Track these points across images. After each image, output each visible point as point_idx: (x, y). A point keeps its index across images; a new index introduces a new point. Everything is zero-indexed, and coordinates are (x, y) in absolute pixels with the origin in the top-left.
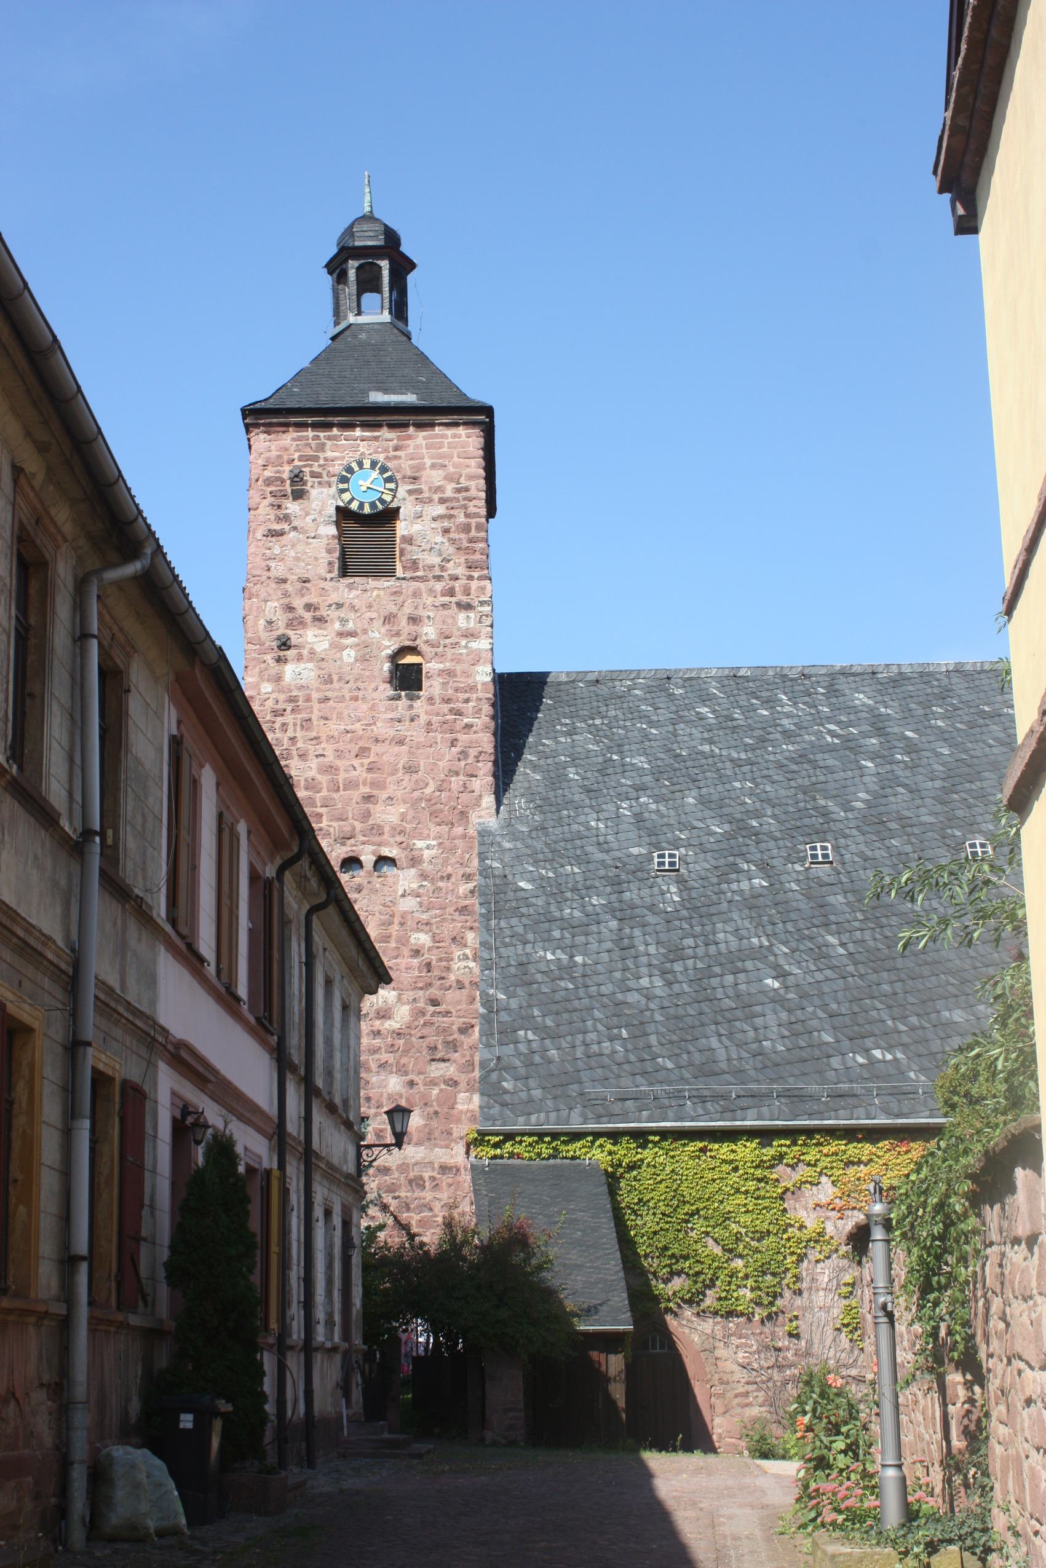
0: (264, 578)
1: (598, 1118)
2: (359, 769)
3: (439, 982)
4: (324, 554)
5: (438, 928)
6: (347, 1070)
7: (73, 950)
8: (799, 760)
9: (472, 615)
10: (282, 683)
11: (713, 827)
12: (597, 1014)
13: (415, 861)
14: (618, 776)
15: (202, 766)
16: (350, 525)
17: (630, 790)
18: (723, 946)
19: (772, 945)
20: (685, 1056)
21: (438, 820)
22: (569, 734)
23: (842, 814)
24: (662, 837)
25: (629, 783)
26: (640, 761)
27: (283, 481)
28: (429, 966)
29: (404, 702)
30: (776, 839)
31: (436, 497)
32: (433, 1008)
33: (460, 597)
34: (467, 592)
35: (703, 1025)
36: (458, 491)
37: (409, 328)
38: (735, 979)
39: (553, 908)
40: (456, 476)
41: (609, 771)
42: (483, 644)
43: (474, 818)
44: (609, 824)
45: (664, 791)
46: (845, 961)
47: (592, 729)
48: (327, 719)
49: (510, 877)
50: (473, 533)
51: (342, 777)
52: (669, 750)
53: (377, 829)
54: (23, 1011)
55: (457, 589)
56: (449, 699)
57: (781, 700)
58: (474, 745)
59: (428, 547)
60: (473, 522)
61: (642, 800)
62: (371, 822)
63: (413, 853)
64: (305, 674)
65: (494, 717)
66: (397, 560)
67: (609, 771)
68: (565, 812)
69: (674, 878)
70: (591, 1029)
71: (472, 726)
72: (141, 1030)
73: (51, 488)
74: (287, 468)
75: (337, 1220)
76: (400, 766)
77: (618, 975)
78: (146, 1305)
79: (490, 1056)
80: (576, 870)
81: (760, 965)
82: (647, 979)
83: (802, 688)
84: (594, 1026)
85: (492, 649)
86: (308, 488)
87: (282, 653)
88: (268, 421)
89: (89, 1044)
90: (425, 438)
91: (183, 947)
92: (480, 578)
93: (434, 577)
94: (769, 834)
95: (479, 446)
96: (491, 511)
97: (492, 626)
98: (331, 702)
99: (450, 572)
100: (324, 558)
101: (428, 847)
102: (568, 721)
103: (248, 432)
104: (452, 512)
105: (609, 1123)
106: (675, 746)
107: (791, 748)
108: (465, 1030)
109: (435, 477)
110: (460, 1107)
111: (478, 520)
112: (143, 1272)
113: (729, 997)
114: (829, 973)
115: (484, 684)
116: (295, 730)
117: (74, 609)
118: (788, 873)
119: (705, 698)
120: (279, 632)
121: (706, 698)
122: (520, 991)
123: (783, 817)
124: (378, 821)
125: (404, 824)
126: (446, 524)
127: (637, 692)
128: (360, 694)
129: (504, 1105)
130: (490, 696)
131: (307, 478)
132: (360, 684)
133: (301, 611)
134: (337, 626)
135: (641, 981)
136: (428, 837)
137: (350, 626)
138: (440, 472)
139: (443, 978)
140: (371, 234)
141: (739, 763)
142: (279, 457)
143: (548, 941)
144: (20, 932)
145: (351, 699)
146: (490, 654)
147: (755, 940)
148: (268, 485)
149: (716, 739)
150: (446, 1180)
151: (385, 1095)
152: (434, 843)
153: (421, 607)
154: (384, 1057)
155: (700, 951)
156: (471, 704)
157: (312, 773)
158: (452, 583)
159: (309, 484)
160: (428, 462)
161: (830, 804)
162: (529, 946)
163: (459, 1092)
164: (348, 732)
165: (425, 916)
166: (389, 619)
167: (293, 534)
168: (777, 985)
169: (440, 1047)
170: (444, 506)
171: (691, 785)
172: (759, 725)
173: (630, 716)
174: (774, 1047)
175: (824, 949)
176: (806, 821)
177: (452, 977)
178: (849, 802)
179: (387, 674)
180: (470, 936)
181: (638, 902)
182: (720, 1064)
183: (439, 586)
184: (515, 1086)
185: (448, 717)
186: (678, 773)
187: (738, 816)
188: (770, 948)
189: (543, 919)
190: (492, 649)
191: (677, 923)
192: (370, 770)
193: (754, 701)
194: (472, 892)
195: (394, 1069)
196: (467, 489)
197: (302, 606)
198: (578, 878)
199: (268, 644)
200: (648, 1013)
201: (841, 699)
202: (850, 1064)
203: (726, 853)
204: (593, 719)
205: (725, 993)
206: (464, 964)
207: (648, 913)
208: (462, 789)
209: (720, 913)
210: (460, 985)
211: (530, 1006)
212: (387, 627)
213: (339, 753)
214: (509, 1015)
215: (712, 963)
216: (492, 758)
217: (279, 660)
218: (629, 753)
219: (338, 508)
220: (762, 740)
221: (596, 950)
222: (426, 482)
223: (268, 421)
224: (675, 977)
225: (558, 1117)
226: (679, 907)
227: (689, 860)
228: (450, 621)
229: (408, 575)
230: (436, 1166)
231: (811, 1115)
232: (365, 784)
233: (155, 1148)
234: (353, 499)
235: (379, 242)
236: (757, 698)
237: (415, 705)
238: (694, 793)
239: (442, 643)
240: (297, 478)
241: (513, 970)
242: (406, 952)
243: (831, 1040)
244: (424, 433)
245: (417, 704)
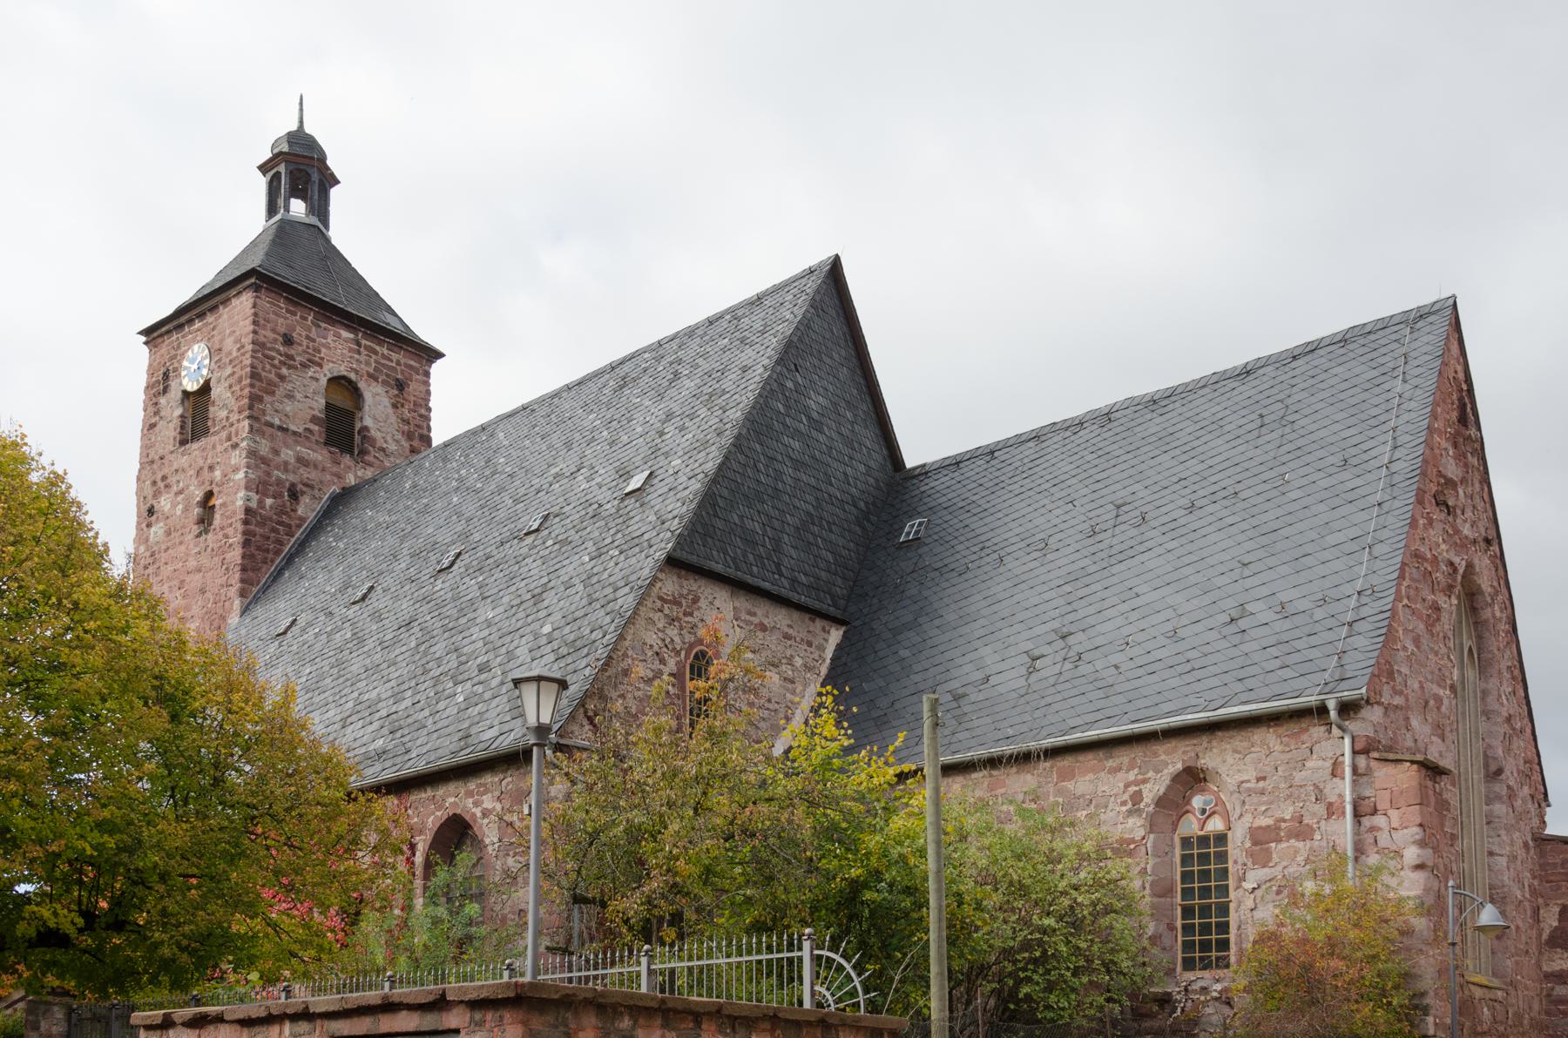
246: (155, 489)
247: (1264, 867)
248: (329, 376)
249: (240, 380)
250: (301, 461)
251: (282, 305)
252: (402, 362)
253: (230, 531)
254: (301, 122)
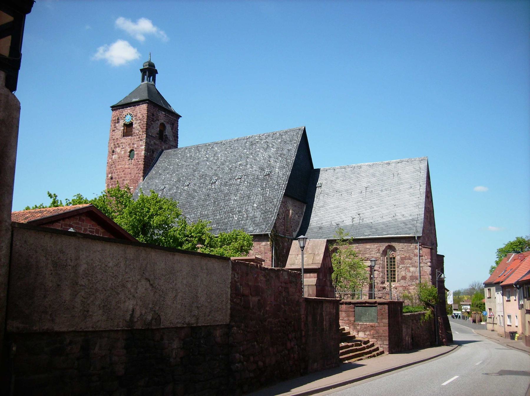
31: (139, 119)
100: (121, 134)
115: (143, 155)
131: (120, 119)
183: (138, 137)
219: (124, 124)
240: (118, 119)
246: (115, 146)
247: (403, 264)
248: (160, 123)
249: (143, 124)
250: (155, 143)
251: (152, 107)
252: (173, 119)
253: (140, 160)
254: (150, 60)
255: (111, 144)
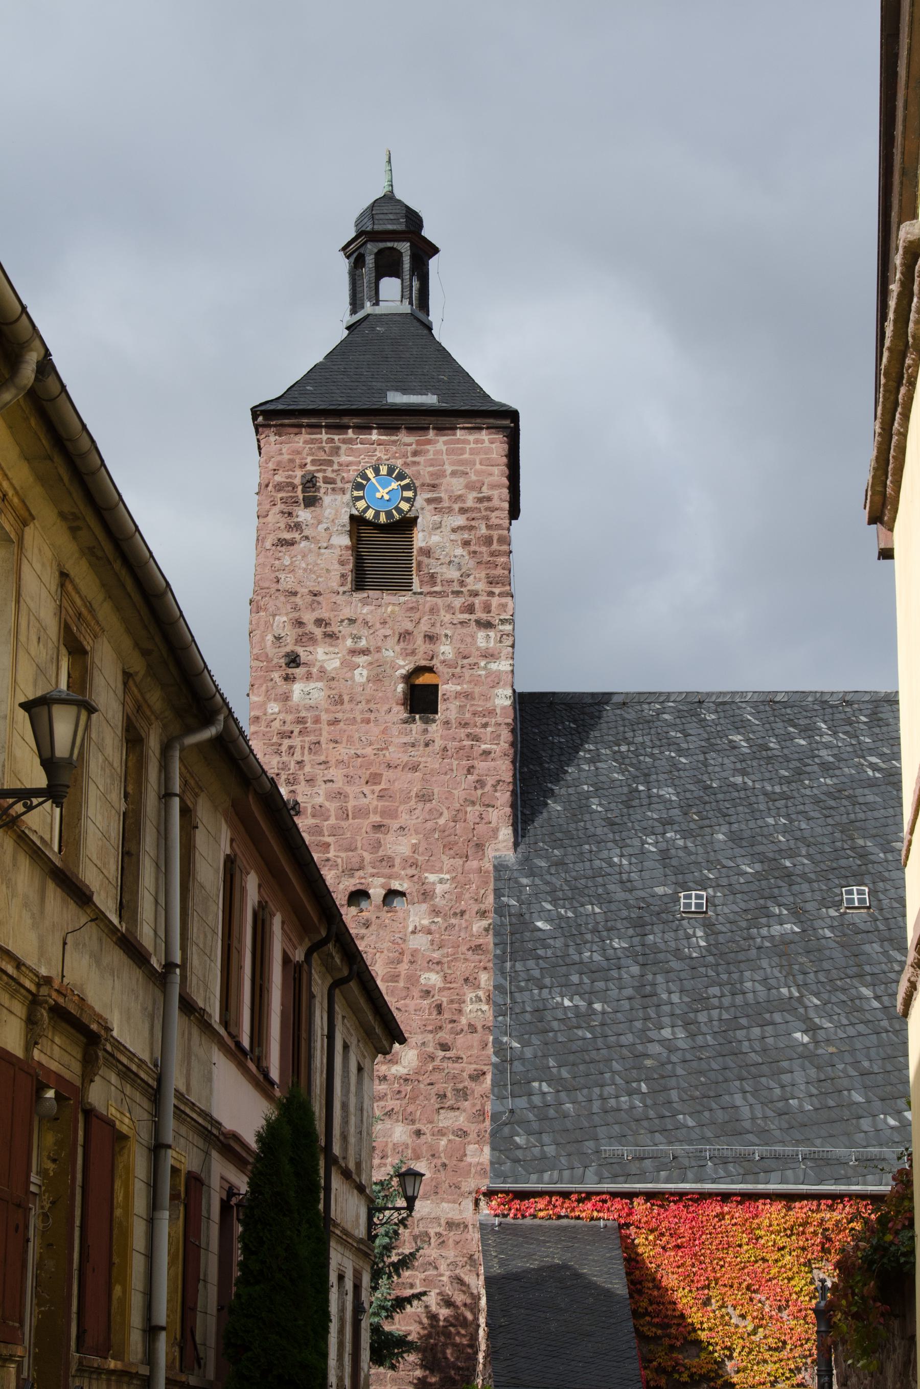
0: (273, 591)
1: (614, 1178)
2: (370, 796)
3: (450, 1026)
4: (337, 566)
5: (449, 968)
6: (361, 1133)
7: (156, 1066)
8: (837, 795)
9: (492, 634)
10: (289, 703)
11: (743, 867)
12: (616, 1066)
13: (426, 895)
14: (644, 809)
15: (248, 873)
16: (367, 532)
17: (656, 824)
18: (750, 996)
19: (802, 996)
20: (707, 1114)
21: (452, 852)
22: (592, 761)
23: (882, 855)
24: (689, 877)
25: (655, 816)
26: (668, 792)
27: (294, 487)
28: (439, 1008)
29: (418, 726)
30: (810, 881)
31: (456, 507)
32: (443, 1053)
33: (481, 615)
34: (487, 609)
35: (726, 1081)
36: (480, 500)
37: (430, 318)
38: (763, 1031)
39: (571, 951)
40: (478, 485)
41: (634, 803)
42: (503, 666)
43: (490, 853)
44: (634, 860)
45: (692, 826)
46: (880, 1015)
47: (618, 757)
48: (336, 742)
49: (527, 917)
50: (495, 546)
51: (351, 804)
52: (699, 781)
53: (388, 861)
54: (124, 1125)
55: (477, 606)
56: (466, 724)
57: (820, 729)
58: (492, 773)
59: (448, 560)
60: (495, 534)
61: (668, 835)
62: (381, 853)
63: (425, 887)
64: (315, 695)
65: (513, 744)
66: (414, 572)
67: (634, 803)
68: (587, 847)
69: (701, 921)
70: (609, 1082)
71: (490, 753)
72: (200, 1124)
73: (149, 679)
74: (299, 473)
75: (349, 1285)
76: (413, 794)
77: (638, 1024)
78: (200, 1367)
79: (501, 1109)
80: (597, 910)
81: (789, 1018)
82: (669, 1030)
83: (843, 716)
84: (612, 1079)
85: (512, 671)
86: (321, 494)
87: (290, 671)
88: (279, 422)
89: (169, 1147)
90: (445, 443)
91: (232, 1045)
92: (501, 595)
93: (453, 592)
94: (804, 875)
95: (504, 453)
96: (514, 512)
97: (513, 646)
98: (342, 724)
99: (469, 588)
100: (337, 571)
101: (441, 881)
102: (592, 747)
103: (257, 432)
104: (473, 523)
105: (625, 1183)
106: (705, 778)
107: (829, 781)
108: (478, 1076)
109: (457, 485)
110: (469, 1159)
111: (500, 532)
112: (198, 1339)
113: (755, 1052)
114: (861, 1028)
115: (504, 708)
116: (303, 754)
117: (160, 771)
118: (822, 919)
119: (739, 724)
120: (288, 649)
121: (740, 726)
122: (535, 1040)
123: (818, 857)
124: (389, 853)
125: (416, 856)
126: (466, 536)
127: (666, 716)
128: (372, 716)
129: (516, 1161)
130: (510, 721)
131: (320, 484)
132: (372, 706)
133: (311, 627)
134: (349, 642)
135: (663, 1031)
136: (441, 871)
137: (363, 643)
138: (461, 480)
139: (455, 1021)
140: (391, 217)
141: (773, 797)
142: (291, 461)
143: (566, 987)
144: (125, 1061)
145: (362, 722)
146: (510, 676)
147: (784, 991)
148: (279, 491)
149: (749, 770)
150: (453, 1236)
151: (390, 1145)
152: (447, 876)
153: (438, 625)
154: (391, 1104)
155: (726, 1001)
156: (489, 729)
157: (320, 800)
158: (471, 599)
159: (322, 491)
160: (449, 469)
161: (869, 844)
162: (545, 992)
163: (469, 1143)
164: (359, 756)
165: (436, 955)
166: (405, 636)
167: (303, 544)
168: (806, 1039)
169: (449, 1095)
170: (465, 516)
171: (721, 821)
172: (796, 756)
173: (658, 743)
174: (801, 1106)
175: (857, 1002)
176: (843, 862)
177: (464, 1021)
178: (889, 842)
179: (401, 695)
180: (484, 977)
181: (662, 946)
182: (743, 1123)
183: (458, 602)
184: (528, 1141)
185: (465, 743)
186: (708, 807)
187: (771, 855)
188: (800, 999)
189: (562, 963)
190: (512, 671)
191: (702, 970)
192: (381, 797)
193: (791, 729)
194: (487, 930)
195: (401, 1118)
196: (489, 499)
197: (312, 621)
198: (599, 918)
199: (275, 661)
200: (669, 1067)
201: (885, 729)
202: (881, 1126)
203: (756, 895)
204: (619, 745)
205: (751, 1047)
206: (476, 1006)
207: (672, 958)
208: (478, 820)
209: (748, 960)
210: (472, 1028)
211: (545, 1056)
212: (402, 645)
213: (349, 779)
214: (523, 1065)
215: (739, 1014)
216: (511, 788)
217: (287, 678)
218: (656, 784)
219: (352, 517)
220: (799, 772)
221: (616, 998)
222: (446, 491)
223: (279, 422)
224: (699, 1028)
225: (572, 1176)
226: (704, 953)
227: (717, 902)
228: (469, 640)
229: (426, 589)
230: (443, 1222)
231: (837, 1181)
232: (375, 813)
233: (208, 1228)
234: (368, 507)
235: (400, 226)
236: (794, 726)
237: (430, 729)
238: (725, 828)
239: (460, 663)
240: (310, 483)
241: (528, 1017)
242: (416, 993)
243: (861, 1100)
244: (445, 438)
245: (433, 727)
255: (274, 615)
